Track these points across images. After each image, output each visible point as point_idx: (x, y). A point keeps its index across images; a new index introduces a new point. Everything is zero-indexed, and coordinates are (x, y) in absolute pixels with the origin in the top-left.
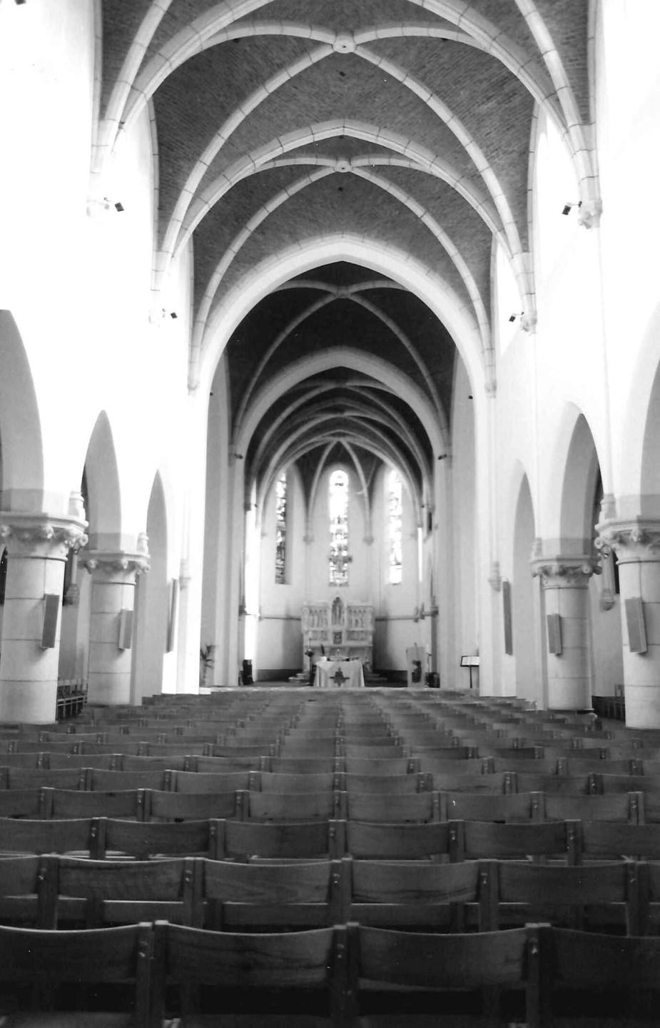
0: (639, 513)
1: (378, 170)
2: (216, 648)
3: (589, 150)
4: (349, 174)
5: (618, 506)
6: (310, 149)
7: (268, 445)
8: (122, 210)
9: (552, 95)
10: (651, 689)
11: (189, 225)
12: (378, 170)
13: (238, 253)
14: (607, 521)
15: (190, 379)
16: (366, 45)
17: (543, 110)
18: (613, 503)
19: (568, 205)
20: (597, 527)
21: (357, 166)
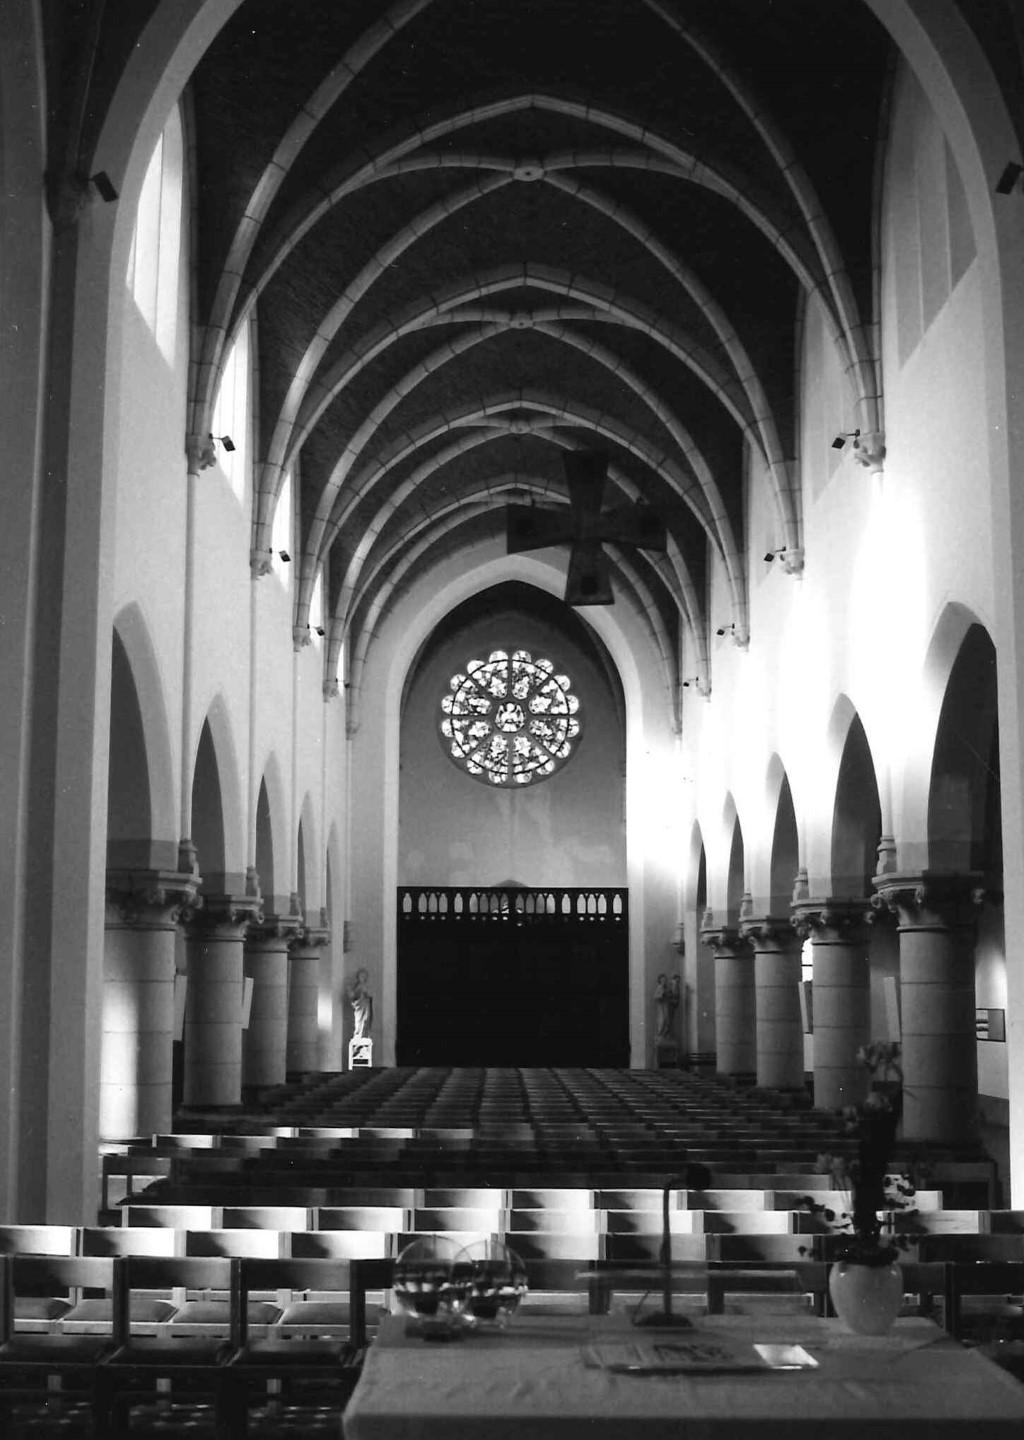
0: (925, 866)
1: (567, 325)
2: (140, 604)
3: (876, 398)
4: (529, 331)
5: (899, 858)
6: (478, 304)
7: (368, 590)
8: (233, 449)
9: (822, 284)
10: (922, 986)
11: (306, 423)
12: (567, 325)
13: (333, 340)
14: (886, 877)
15: (348, 723)
16: (560, 173)
17: (816, 304)
18: (892, 851)
19: (841, 437)
20: (875, 880)
21: (541, 322)
